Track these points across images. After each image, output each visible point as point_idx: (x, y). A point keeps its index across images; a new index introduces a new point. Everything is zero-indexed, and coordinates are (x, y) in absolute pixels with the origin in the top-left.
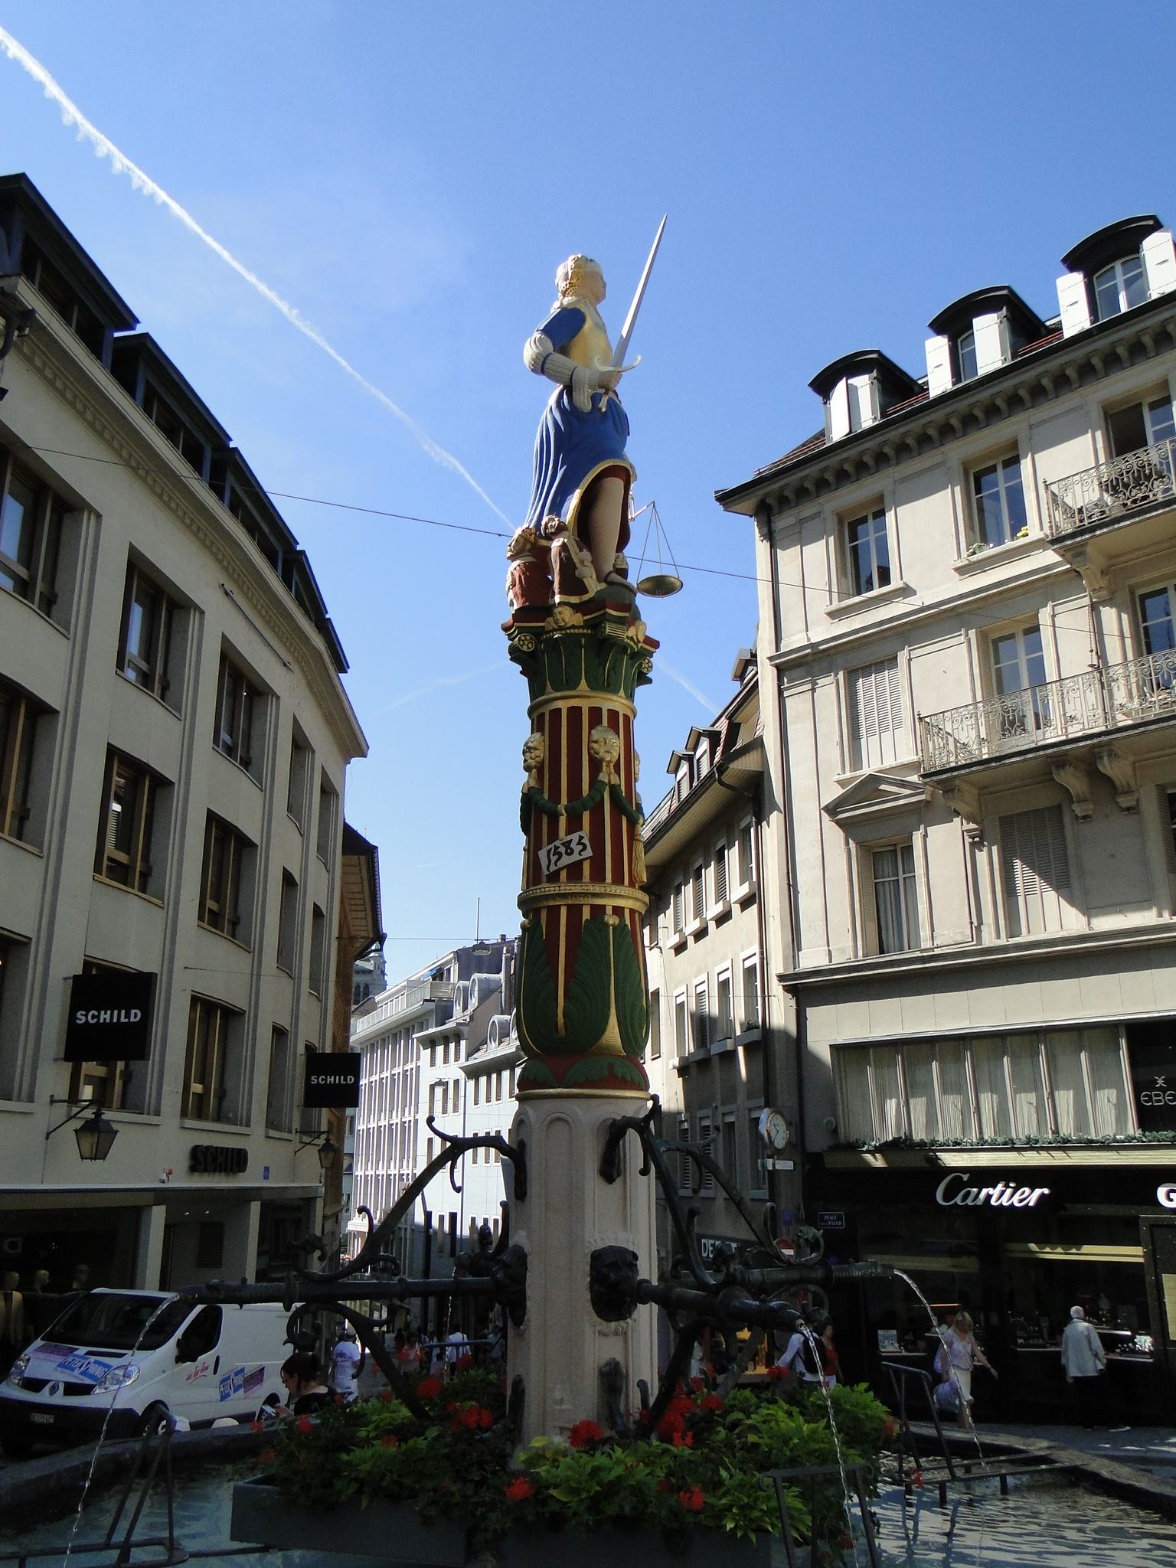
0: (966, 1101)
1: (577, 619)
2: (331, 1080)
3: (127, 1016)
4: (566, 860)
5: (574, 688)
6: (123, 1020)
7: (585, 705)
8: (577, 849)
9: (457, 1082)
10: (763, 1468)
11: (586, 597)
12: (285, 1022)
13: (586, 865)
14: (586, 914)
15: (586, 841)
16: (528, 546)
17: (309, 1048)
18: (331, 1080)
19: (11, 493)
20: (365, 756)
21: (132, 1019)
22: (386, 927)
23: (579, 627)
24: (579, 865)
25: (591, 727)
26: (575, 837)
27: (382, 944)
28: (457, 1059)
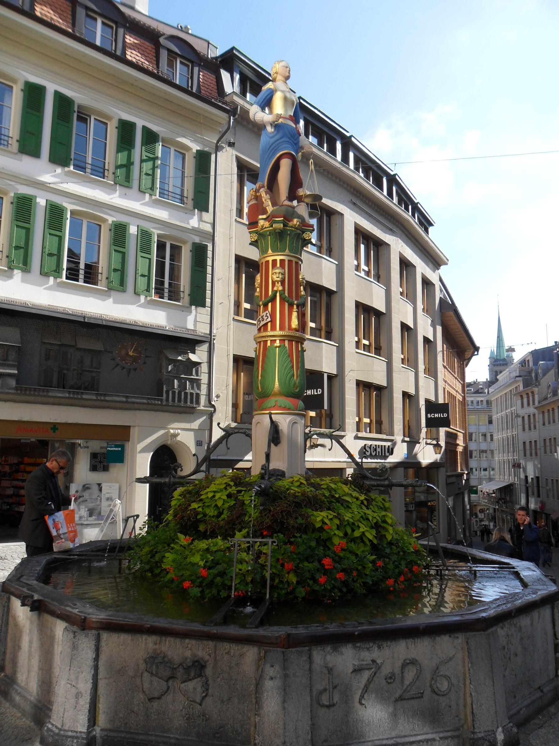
0: (289, 409)
1: (267, 224)
2: (436, 415)
3: (317, 392)
4: (262, 323)
5: (267, 253)
6: (315, 393)
7: (270, 259)
8: (265, 318)
9: (534, 415)
10: (410, 572)
11: (268, 214)
12: (411, 391)
13: (269, 324)
14: (269, 344)
15: (268, 315)
16: (253, 197)
17: (427, 401)
18: (436, 415)
19: (247, 180)
20: (447, 264)
21: (319, 393)
22: (478, 344)
23: (268, 227)
24: (267, 324)
25: (273, 268)
26: (265, 314)
27: (478, 352)
28: (534, 404)
